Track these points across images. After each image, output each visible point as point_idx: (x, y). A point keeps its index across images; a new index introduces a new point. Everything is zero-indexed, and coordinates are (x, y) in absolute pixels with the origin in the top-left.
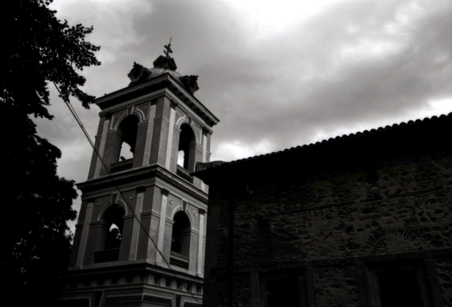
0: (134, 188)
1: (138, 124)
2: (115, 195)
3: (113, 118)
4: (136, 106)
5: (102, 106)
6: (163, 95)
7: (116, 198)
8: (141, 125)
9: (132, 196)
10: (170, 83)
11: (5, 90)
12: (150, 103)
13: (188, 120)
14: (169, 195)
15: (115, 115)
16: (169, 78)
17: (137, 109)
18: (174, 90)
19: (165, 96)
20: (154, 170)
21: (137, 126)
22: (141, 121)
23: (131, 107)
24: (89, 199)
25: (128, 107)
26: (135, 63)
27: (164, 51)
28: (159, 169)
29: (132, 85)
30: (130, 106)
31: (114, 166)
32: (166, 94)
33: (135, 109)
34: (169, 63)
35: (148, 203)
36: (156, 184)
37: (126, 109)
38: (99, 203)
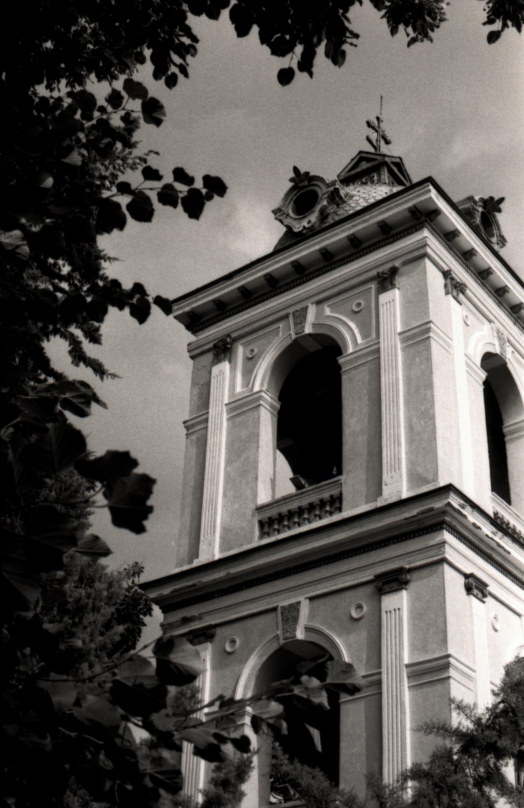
0: (367, 576)
1: (341, 360)
2: (291, 614)
3: (240, 352)
4: (319, 303)
5: (194, 322)
6: (419, 256)
7: (296, 619)
8: (351, 361)
9: (359, 607)
10: (437, 212)
11: (292, 12)
12: (373, 286)
13: (496, 342)
14: (489, 600)
15: (245, 345)
16: (433, 194)
17: (328, 311)
18: (449, 237)
19: (426, 255)
20: (438, 504)
21: (339, 368)
22: (351, 350)
23: (305, 309)
24: (190, 632)
25: (291, 310)
26: (296, 170)
27: (368, 140)
28: (455, 501)
29: (291, 239)
30: (299, 307)
31: (273, 513)
32: (429, 250)
33: (319, 314)
34: (391, 172)
35: (433, 622)
36: (447, 556)
37: (286, 316)
38: (233, 642)
